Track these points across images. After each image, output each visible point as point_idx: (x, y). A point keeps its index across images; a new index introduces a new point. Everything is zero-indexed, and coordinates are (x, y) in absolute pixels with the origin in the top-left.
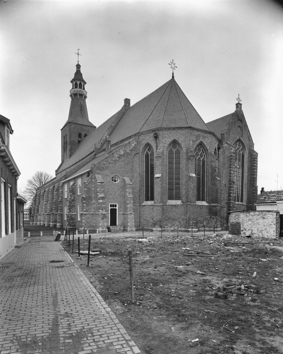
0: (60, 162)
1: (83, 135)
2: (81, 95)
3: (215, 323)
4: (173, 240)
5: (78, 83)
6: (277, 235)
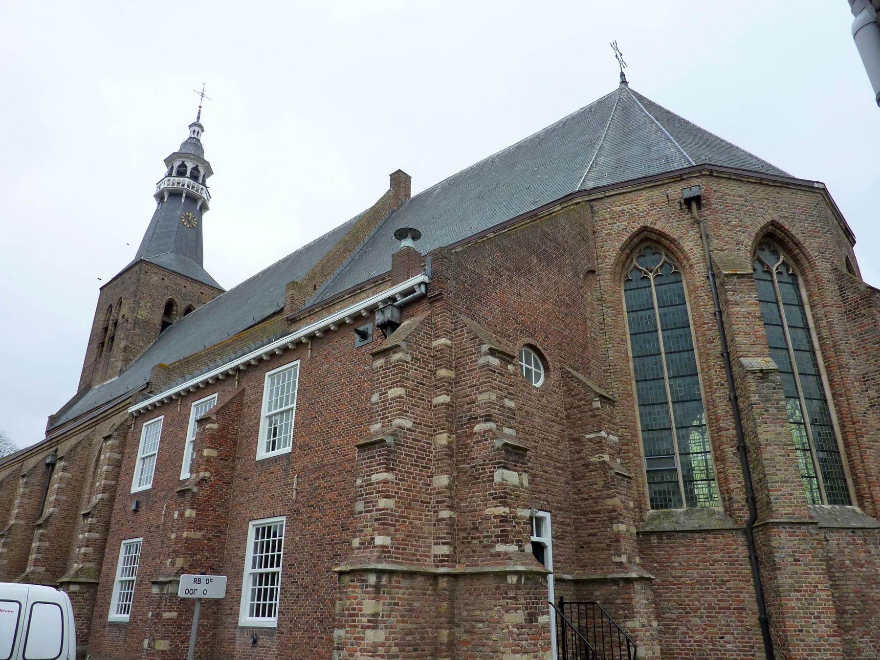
0: (74, 392)
2: (193, 199)
5: (190, 166)
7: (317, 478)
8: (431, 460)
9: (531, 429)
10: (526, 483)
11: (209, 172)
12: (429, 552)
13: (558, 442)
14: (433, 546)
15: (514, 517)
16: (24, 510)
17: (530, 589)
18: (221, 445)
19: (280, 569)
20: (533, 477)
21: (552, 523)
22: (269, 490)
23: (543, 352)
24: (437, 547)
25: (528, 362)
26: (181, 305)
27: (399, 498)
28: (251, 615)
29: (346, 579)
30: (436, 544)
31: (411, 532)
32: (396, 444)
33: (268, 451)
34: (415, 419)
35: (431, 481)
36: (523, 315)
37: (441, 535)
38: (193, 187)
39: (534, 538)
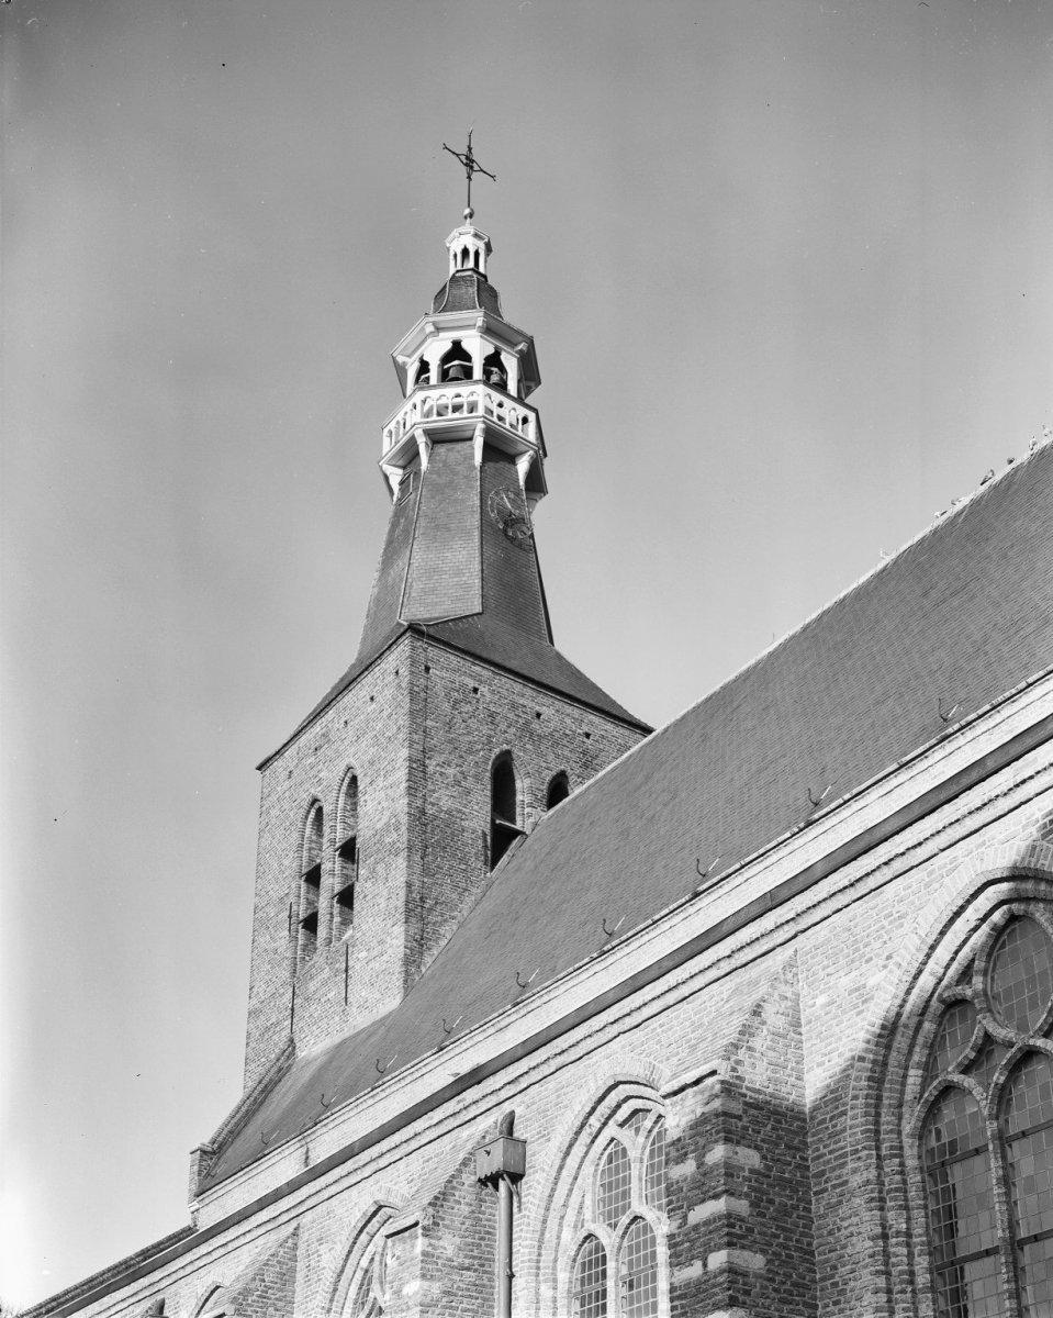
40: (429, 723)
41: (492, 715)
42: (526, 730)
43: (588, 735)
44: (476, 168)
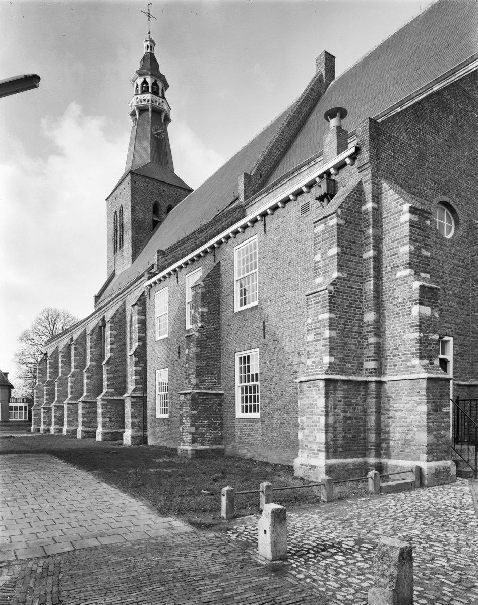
1: (163, 208)
3: (386, 443)
4: (314, 580)
6: (457, 372)
7: (278, 321)
8: (362, 302)
9: (441, 274)
10: (437, 315)
11: (166, 86)
12: (362, 367)
13: (463, 283)
14: (365, 363)
15: (426, 340)
16: (94, 356)
17: (437, 389)
18: (209, 303)
19: (258, 383)
20: (441, 311)
21: (454, 344)
22: (245, 332)
23: (455, 207)
24: (368, 363)
25: (442, 218)
26: (164, 205)
27: (339, 330)
28: (243, 412)
29: (305, 385)
30: (367, 361)
31: (349, 353)
32: (335, 291)
33: (241, 305)
34: (350, 271)
35: (362, 318)
36: (439, 175)
37: (370, 355)
38: (156, 102)
39: (441, 356)
40: (135, 196)
41: (151, 192)
42: (161, 195)
43: (177, 194)
44: (151, 16)
